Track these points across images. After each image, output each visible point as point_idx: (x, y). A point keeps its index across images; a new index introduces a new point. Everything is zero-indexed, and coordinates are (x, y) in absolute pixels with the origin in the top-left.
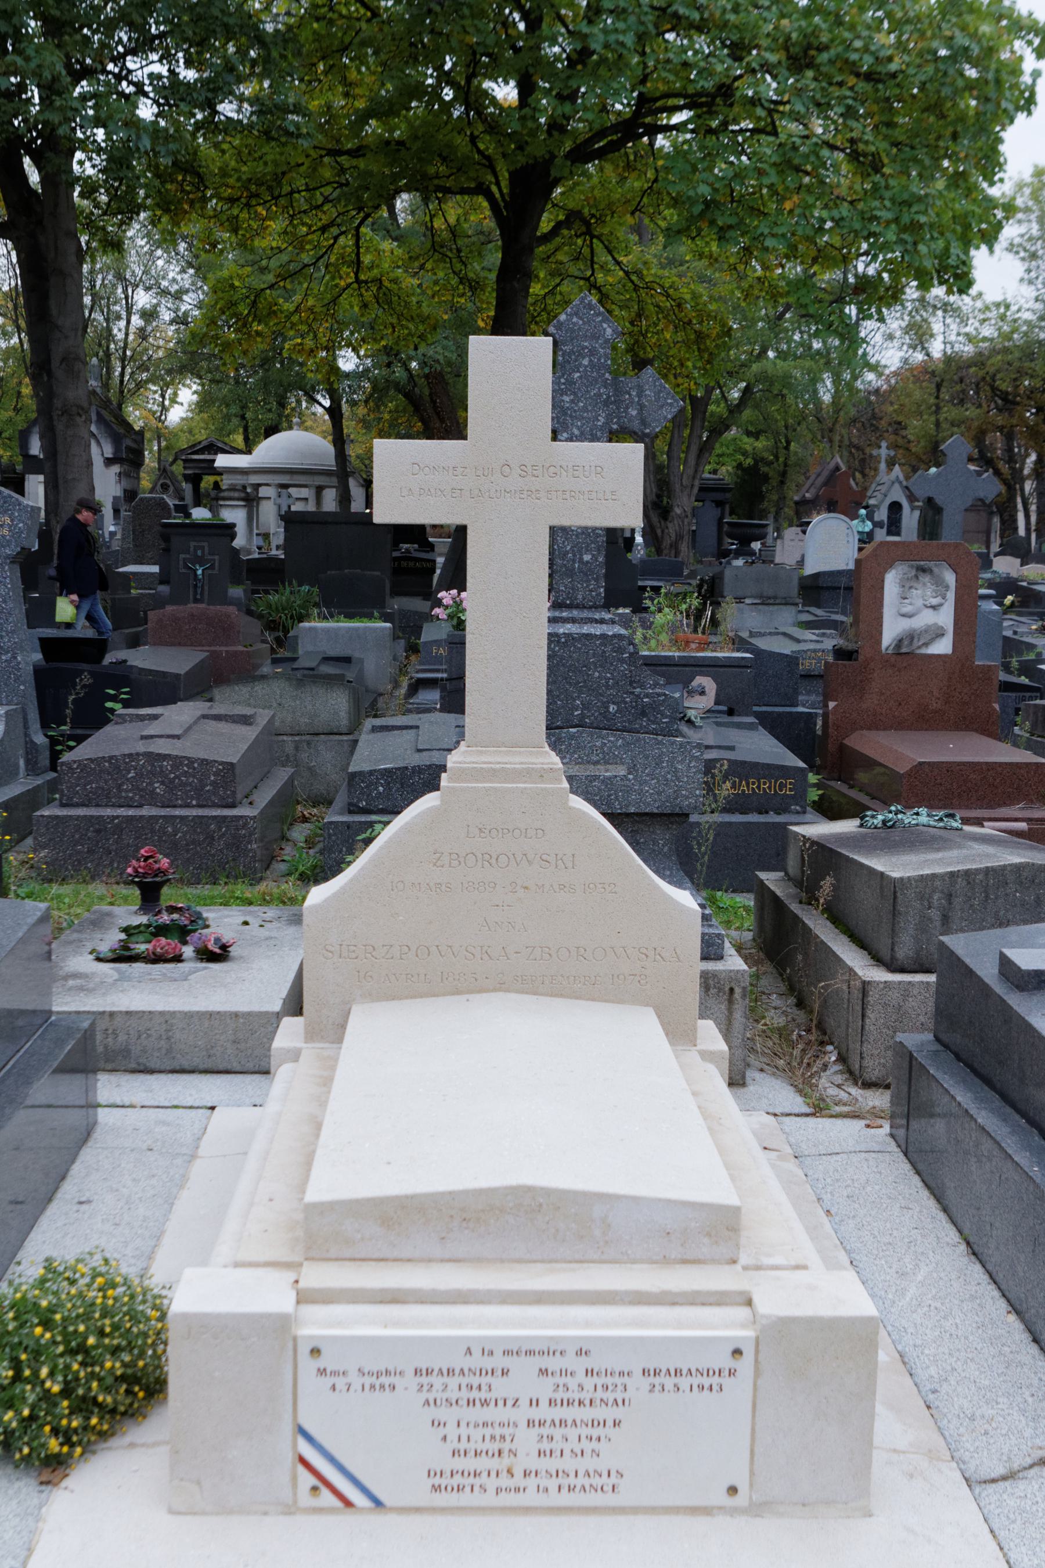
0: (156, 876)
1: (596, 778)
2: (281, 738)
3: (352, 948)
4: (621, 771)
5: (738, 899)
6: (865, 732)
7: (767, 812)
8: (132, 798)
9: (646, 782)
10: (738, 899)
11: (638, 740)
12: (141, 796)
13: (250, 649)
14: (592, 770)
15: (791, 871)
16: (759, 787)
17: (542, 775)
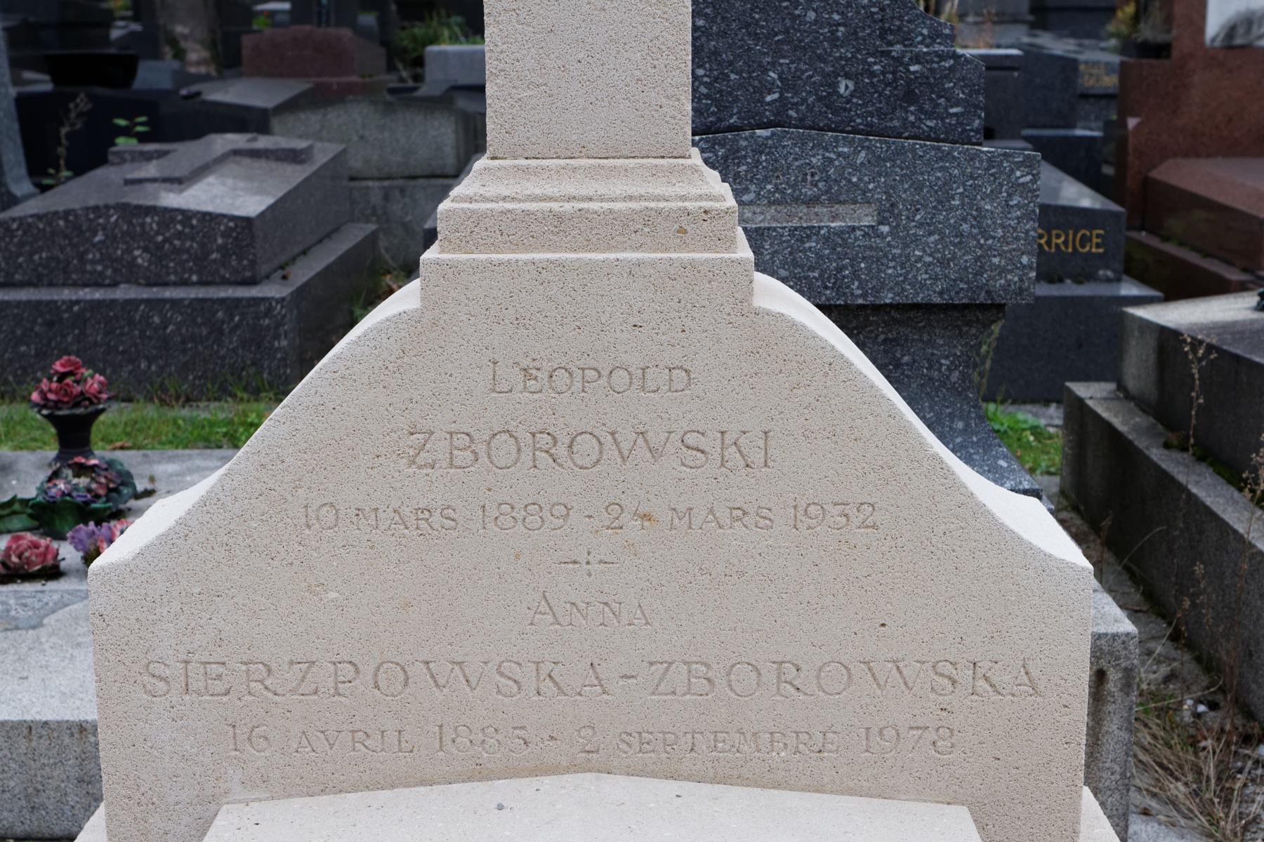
0: (77, 405)
1: (812, 232)
2: (364, 183)
3: (215, 669)
4: (865, 217)
5: (1021, 416)
6: (1179, 160)
7: (1061, 280)
8: (101, 274)
9: (916, 239)
10: (1021, 416)
11: (900, 152)
12: (115, 270)
13: (367, 80)
14: (802, 217)
15: (1131, 384)
16: (1049, 243)
17: (685, 226)
